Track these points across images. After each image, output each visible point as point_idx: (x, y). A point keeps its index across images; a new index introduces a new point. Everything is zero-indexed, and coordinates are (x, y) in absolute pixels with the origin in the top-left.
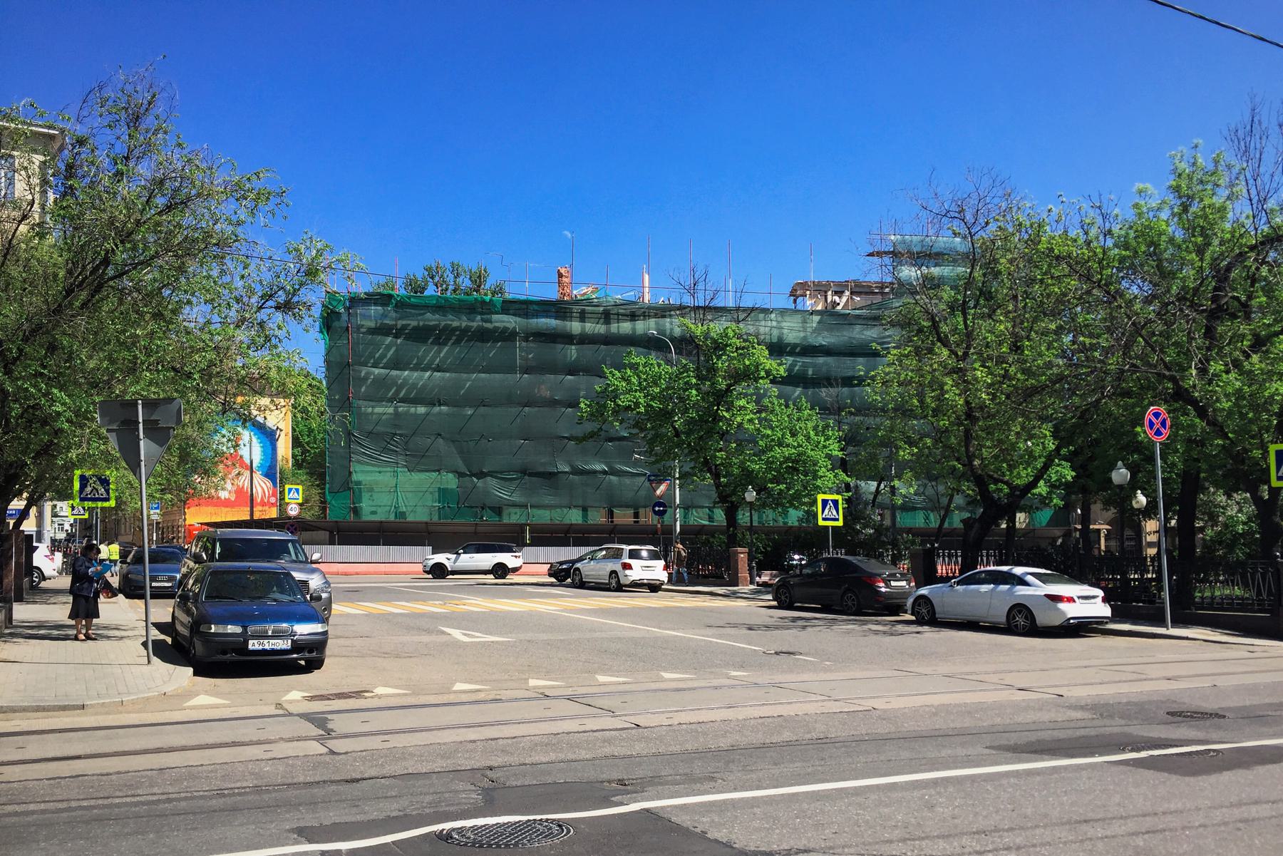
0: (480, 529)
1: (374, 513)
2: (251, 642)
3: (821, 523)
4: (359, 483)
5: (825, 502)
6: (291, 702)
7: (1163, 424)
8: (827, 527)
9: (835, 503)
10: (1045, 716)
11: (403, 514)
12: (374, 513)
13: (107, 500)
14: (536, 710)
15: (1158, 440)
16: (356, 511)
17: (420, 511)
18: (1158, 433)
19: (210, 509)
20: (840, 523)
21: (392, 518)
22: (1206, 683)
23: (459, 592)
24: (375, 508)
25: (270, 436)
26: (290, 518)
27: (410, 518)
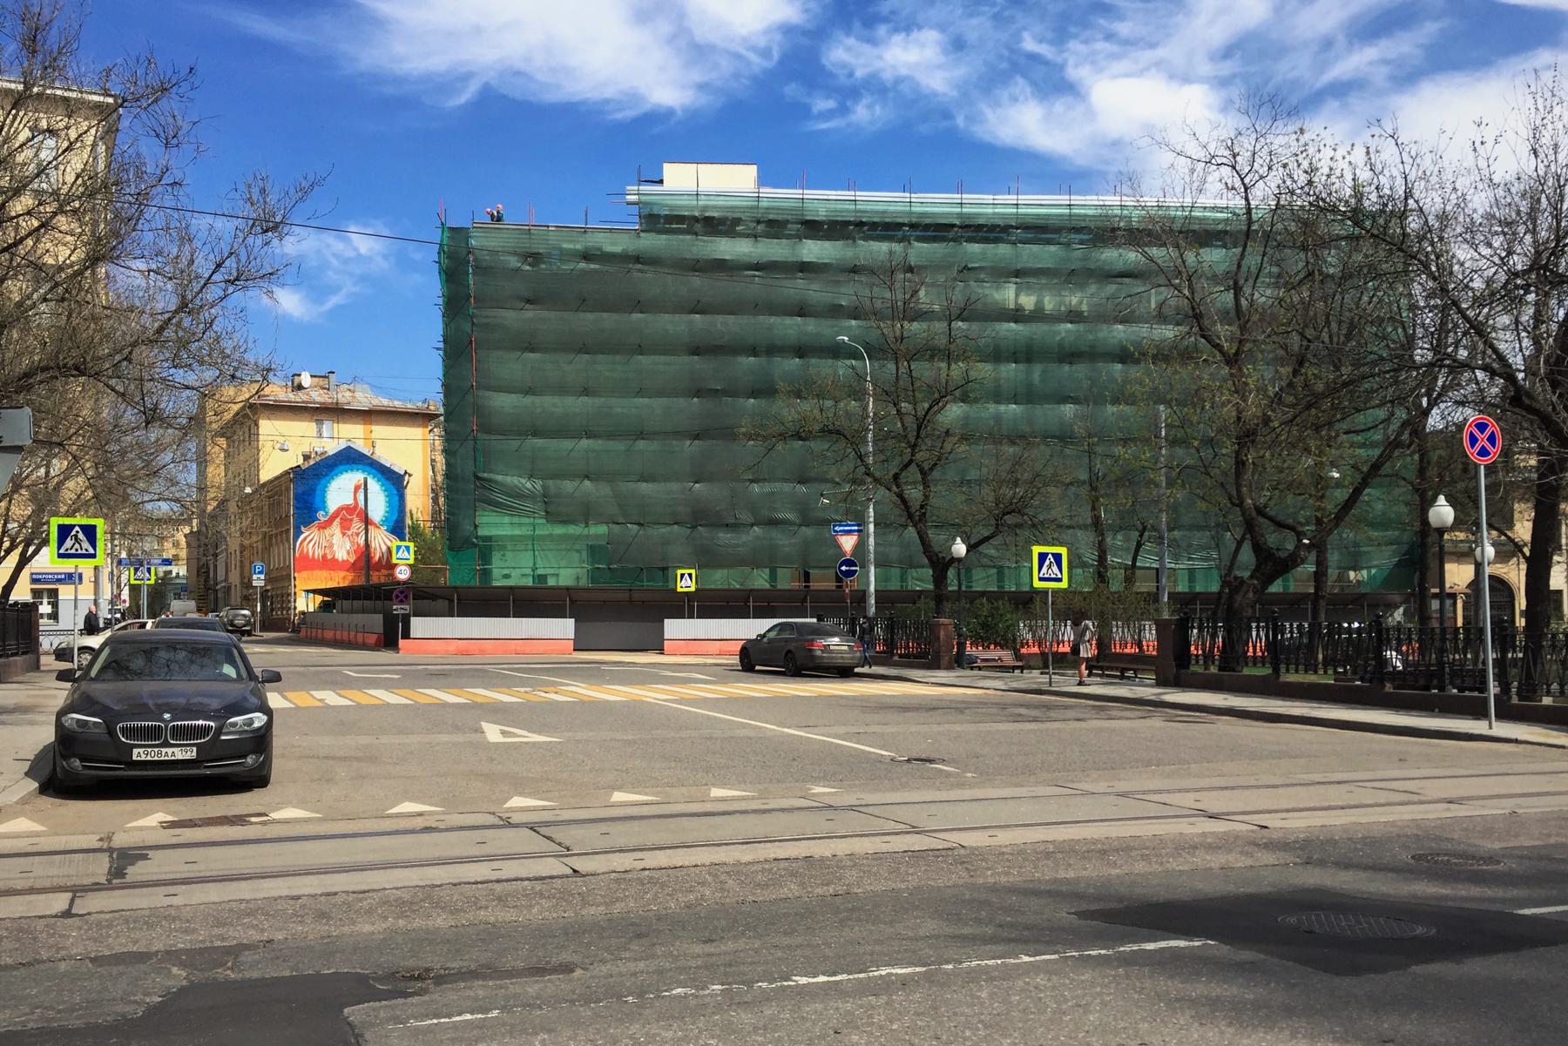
0: (636, 596)
1: (507, 576)
2: (135, 751)
3: (1037, 584)
4: (489, 539)
5: (1043, 557)
6: (512, 810)
7: (1492, 439)
8: (1045, 592)
9: (1058, 557)
10: (1238, 861)
11: (543, 578)
12: (507, 576)
13: (1060, 580)
14: (819, 823)
15: (1482, 463)
16: (486, 574)
17: (567, 573)
18: (1483, 452)
19: (324, 573)
20: (1064, 585)
21: (529, 582)
22: (1506, 806)
23: (565, 677)
24: (511, 571)
25: (395, 481)
26: (399, 583)
27: (551, 582)
